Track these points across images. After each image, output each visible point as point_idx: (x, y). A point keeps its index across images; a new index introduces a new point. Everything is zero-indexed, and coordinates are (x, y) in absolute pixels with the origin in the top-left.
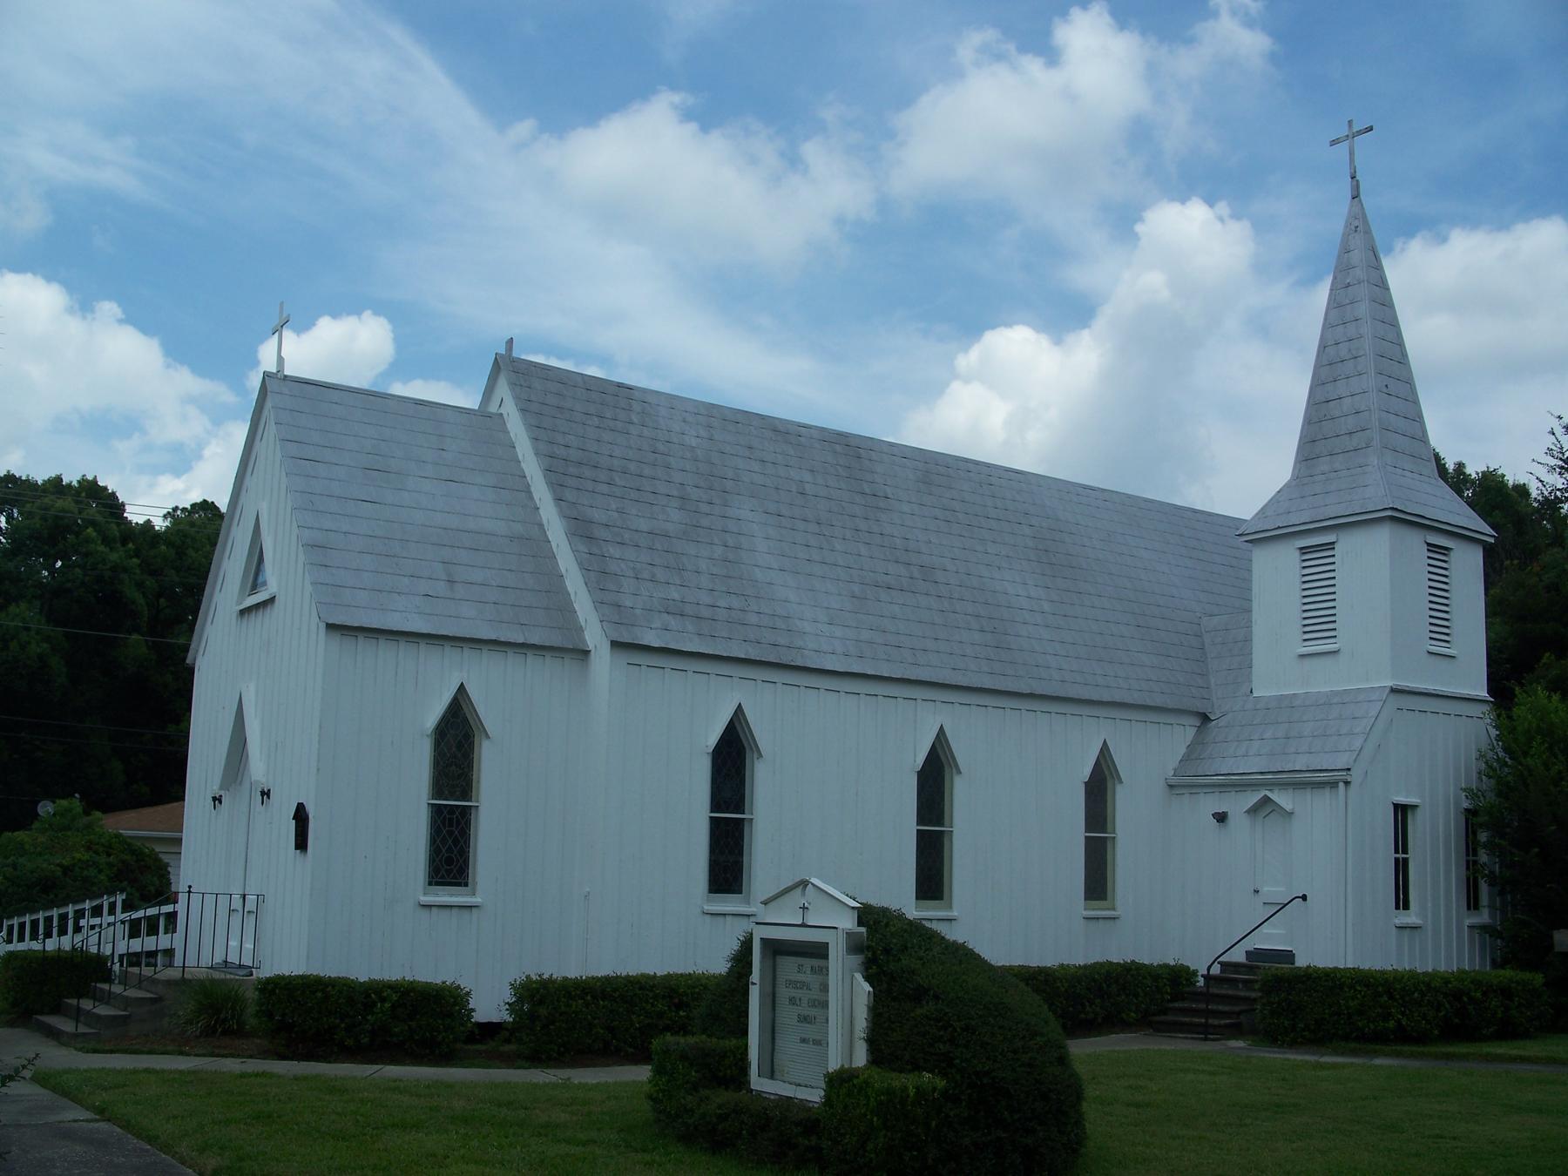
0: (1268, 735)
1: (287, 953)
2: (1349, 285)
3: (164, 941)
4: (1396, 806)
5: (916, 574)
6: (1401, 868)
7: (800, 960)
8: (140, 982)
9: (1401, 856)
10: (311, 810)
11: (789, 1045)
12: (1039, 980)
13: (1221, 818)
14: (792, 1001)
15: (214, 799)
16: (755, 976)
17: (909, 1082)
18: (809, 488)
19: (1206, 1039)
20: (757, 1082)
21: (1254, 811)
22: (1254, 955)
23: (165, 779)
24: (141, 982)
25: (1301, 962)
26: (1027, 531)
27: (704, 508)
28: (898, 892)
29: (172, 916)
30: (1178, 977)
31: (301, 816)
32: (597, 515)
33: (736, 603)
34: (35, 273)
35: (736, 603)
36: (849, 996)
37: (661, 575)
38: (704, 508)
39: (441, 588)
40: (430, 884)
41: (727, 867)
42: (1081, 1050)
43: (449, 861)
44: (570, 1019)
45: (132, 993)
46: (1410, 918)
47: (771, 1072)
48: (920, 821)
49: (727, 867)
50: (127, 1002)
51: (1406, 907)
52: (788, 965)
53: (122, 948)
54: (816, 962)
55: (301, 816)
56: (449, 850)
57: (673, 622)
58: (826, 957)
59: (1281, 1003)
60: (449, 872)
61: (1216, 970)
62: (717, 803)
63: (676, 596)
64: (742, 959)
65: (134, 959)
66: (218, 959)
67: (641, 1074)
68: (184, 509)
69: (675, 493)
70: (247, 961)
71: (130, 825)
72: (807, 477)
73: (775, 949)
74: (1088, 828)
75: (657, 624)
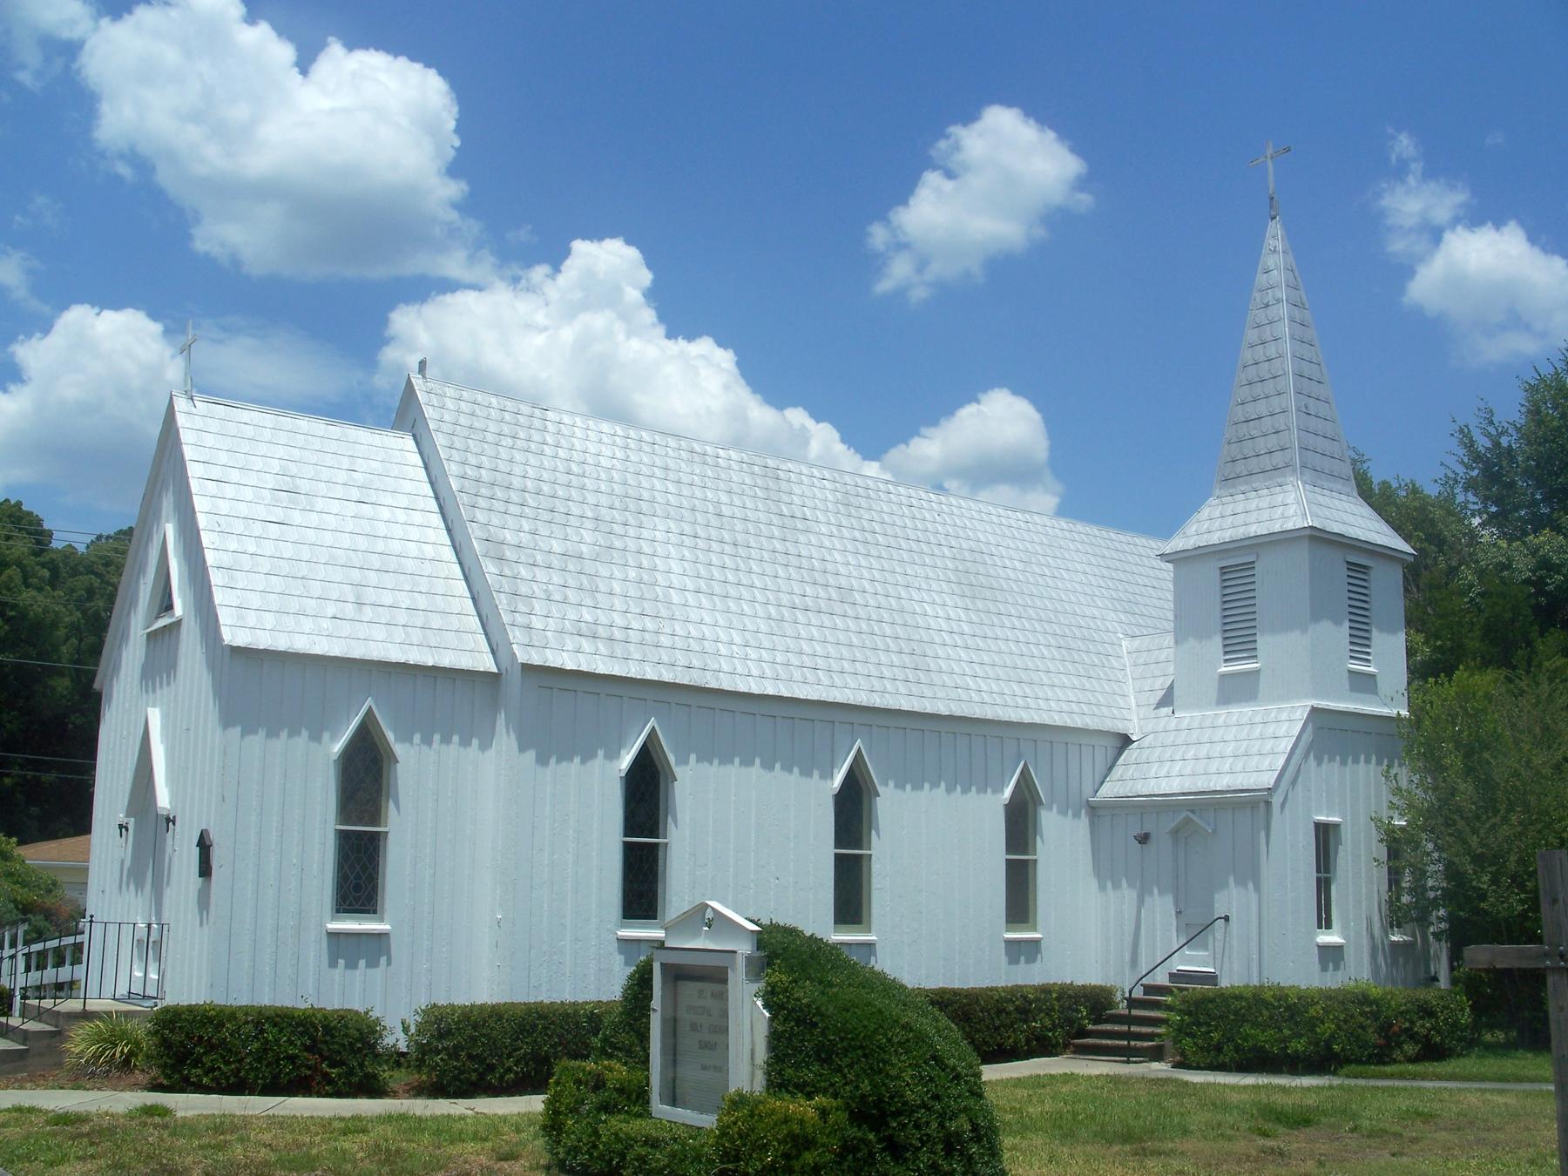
0: (1190, 755)
1: (189, 983)
2: (1267, 306)
3: (65, 974)
4: (1318, 825)
5: (834, 595)
6: (205, 870)
7: (699, 985)
8: (40, 1014)
9: (1322, 875)
10: (214, 837)
11: (690, 1072)
12: (945, 1001)
13: (1144, 839)
14: (694, 1027)
15: (121, 826)
16: (656, 1003)
17: (804, 1109)
18: (726, 510)
19: (1128, 1062)
20: (659, 1108)
21: (1175, 833)
22: (1176, 977)
23: (69, 811)
24: (40, 1015)
25: (1224, 983)
26: (946, 551)
27: (618, 529)
28: (814, 917)
29: (78, 947)
30: (1097, 1001)
31: (204, 845)
32: (509, 536)
33: (650, 624)
34: (136, 308)
35: (650, 624)
36: (749, 1019)
37: (572, 596)
38: (618, 529)
39: (350, 610)
40: (338, 911)
41: (641, 887)
42: (991, 1073)
43: (357, 888)
44: (474, 1051)
45: (32, 1026)
46: (1331, 938)
47: (673, 1099)
48: (838, 844)
49: (641, 887)
50: (25, 1036)
51: (1328, 926)
52: (689, 990)
53: (21, 981)
54: (716, 987)
55: (204, 845)
56: (358, 877)
57: (586, 645)
58: (725, 981)
59: (1222, 1028)
60: (357, 899)
61: (1138, 993)
62: (631, 827)
63: (588, 618)
64: (641, 983)
65: (40, 990)
66: (122, 991)
67: (534, 1104)
68: (108, 537)
69: (590, 514)
70: (151, 992)
71: (40, 856)
72: (724, 498)
73: (678, 975)
74: (839, 843)
75: (570, 646)
